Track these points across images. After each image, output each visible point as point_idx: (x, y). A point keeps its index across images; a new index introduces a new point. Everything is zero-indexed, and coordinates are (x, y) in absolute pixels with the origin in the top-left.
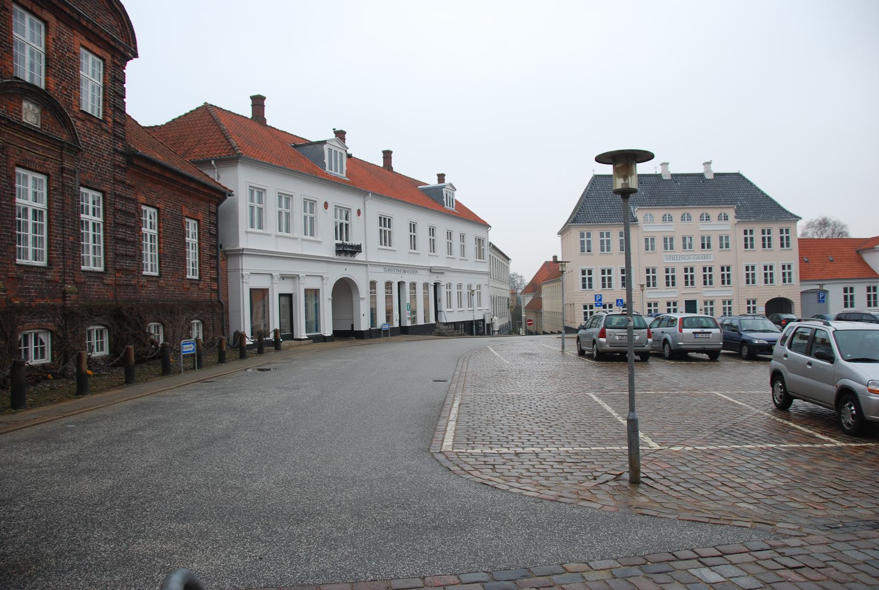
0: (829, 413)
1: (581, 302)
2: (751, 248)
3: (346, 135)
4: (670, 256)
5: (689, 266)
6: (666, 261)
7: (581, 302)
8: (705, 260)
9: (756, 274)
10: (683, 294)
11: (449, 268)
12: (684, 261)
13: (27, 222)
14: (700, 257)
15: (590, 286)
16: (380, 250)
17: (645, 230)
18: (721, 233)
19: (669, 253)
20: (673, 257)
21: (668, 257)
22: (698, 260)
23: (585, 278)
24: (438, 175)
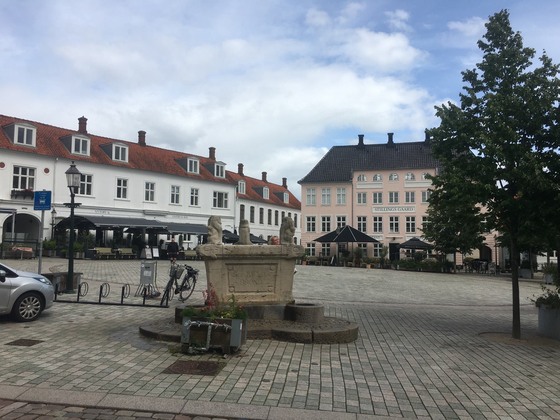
0: (7, 261)
1: (305, 241)
2: (363, 203)
3: (146, 135)
4: (378, 208)
5: (394, 215)
6: (374, 212)
7: (305, 241)
8: (408, 211)
9: (389, 220)
10: (386, 238)
11: (169, 212)
12: (391, 212)
13: (14, 173)
14: (404, 209)
15: (314, 230)
16: (115, 201)
17: (406, 186)
18: (375, 191)
19: (378, 205)
20: (381, 208)
21: (377, 209)
22: (402, 211)
23: (409, 223)
24: (359, 136)
